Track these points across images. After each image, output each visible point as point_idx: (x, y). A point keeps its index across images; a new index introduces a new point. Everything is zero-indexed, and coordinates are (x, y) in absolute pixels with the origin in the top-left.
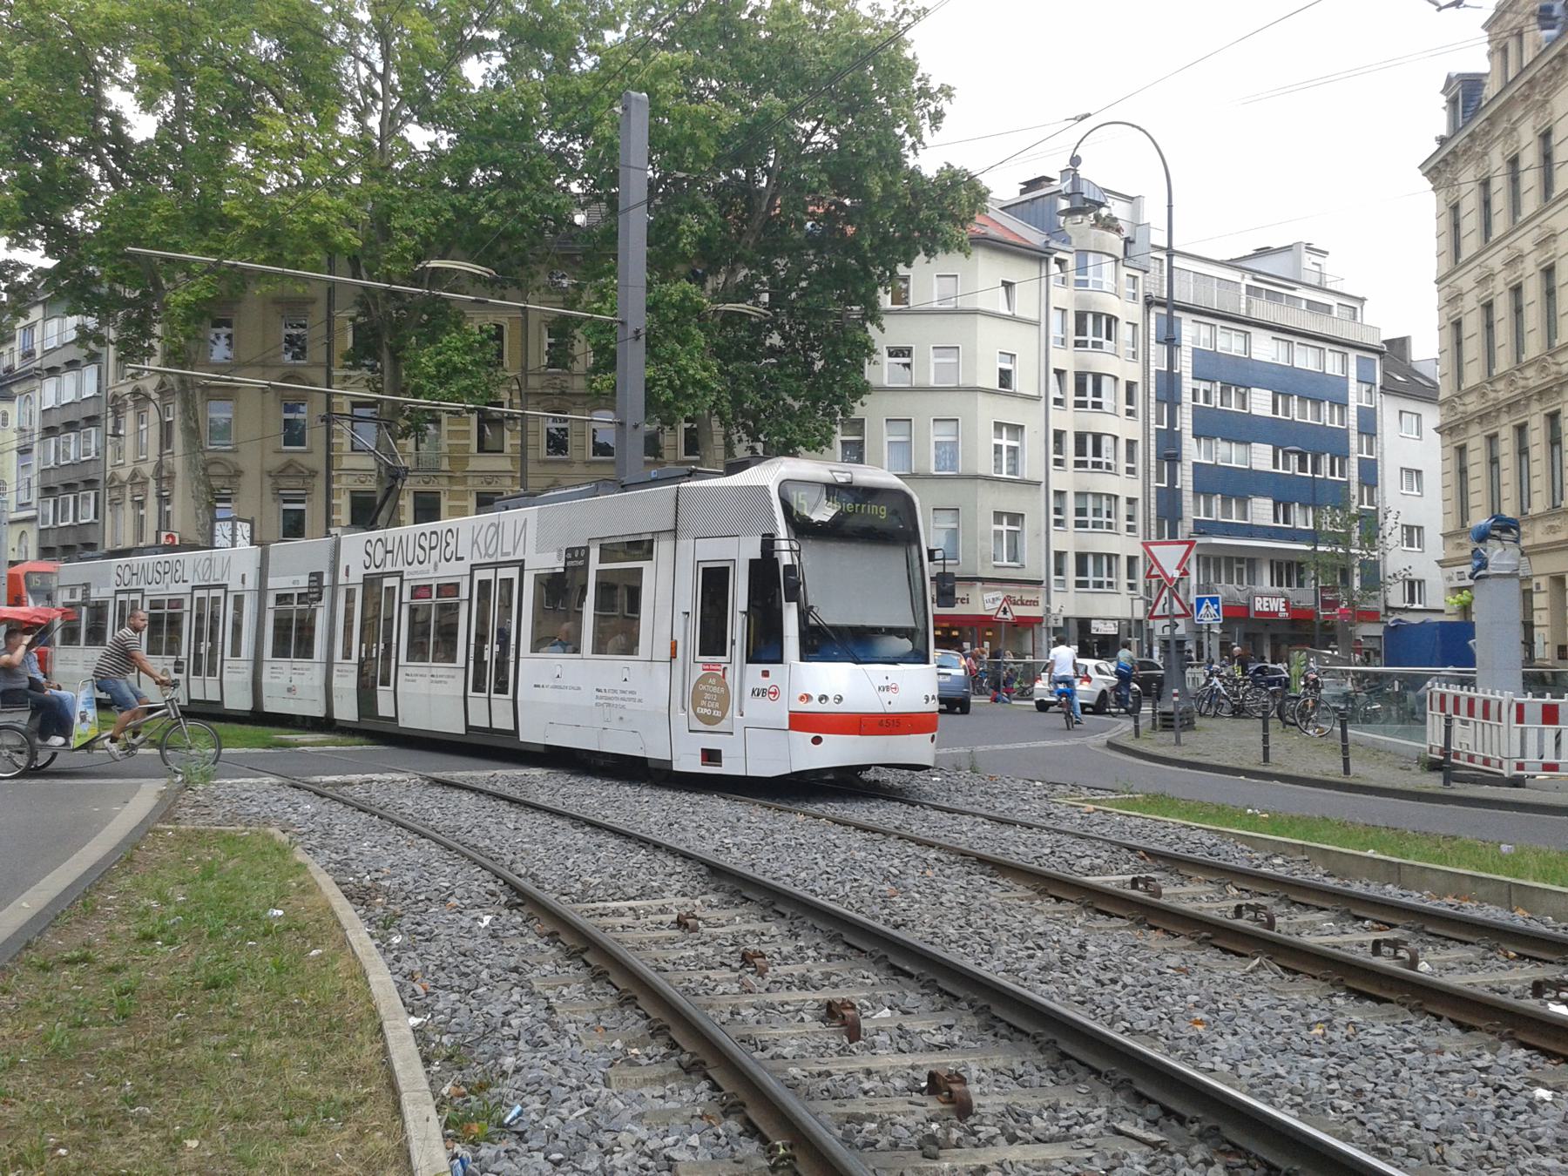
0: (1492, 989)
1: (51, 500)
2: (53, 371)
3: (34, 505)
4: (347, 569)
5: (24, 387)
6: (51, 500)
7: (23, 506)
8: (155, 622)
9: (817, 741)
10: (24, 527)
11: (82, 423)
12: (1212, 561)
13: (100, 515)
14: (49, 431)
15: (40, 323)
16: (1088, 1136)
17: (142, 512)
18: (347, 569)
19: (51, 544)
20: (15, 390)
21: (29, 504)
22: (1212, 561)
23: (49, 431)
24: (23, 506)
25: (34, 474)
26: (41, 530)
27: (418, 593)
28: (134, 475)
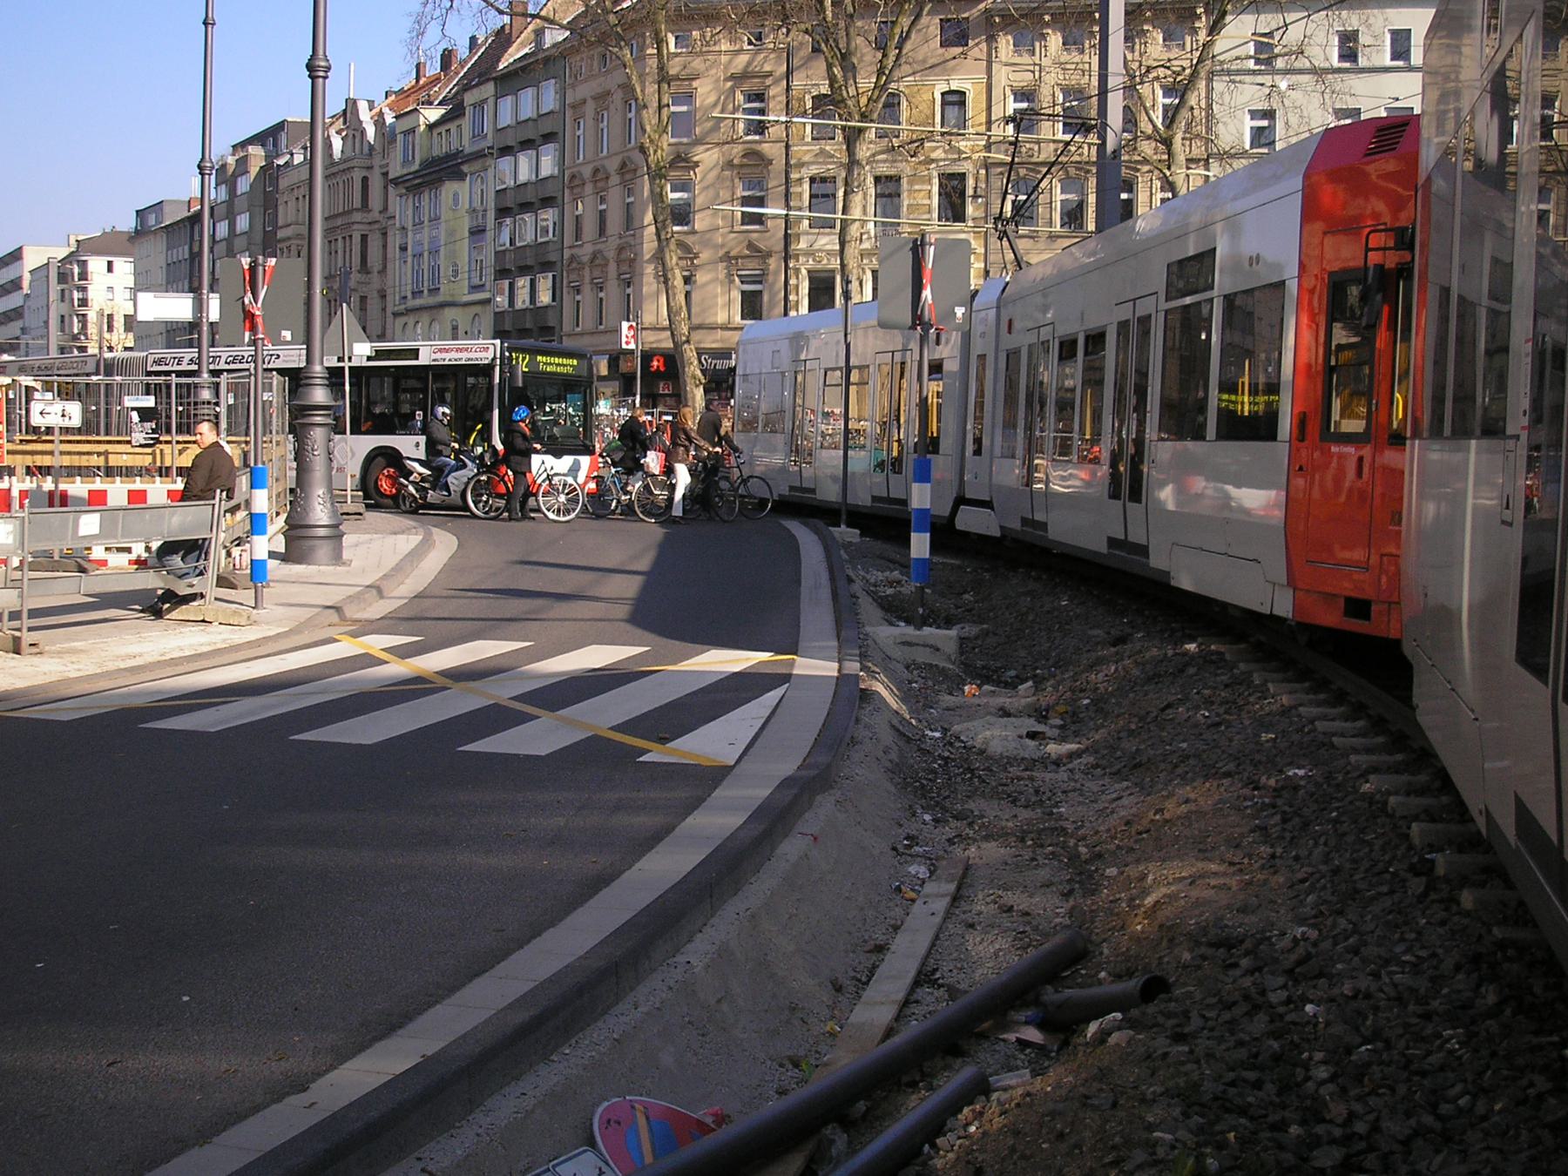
1: (507, 282)
2: (506, 151)
3: (488, 287)
4: (1010, 322)
5: (477, 165)
6: (507, 282)
7: (475, 288)
9: (1358, 608)
10: (477, 309)
12: (1265, 123)
13: (558, 299)
14: (503, 212)
15: (491, 101)
17: (578, 298)
18: (1010, 322)
19: (508, 327)
20: (465, 168)
21: (483, 286)
22: (1265, 123)
23: (503, 212)
24: (475, 288)
25: (489, 258)
26: (496, 314)
27: (1407, 240)
28: (594, 256)
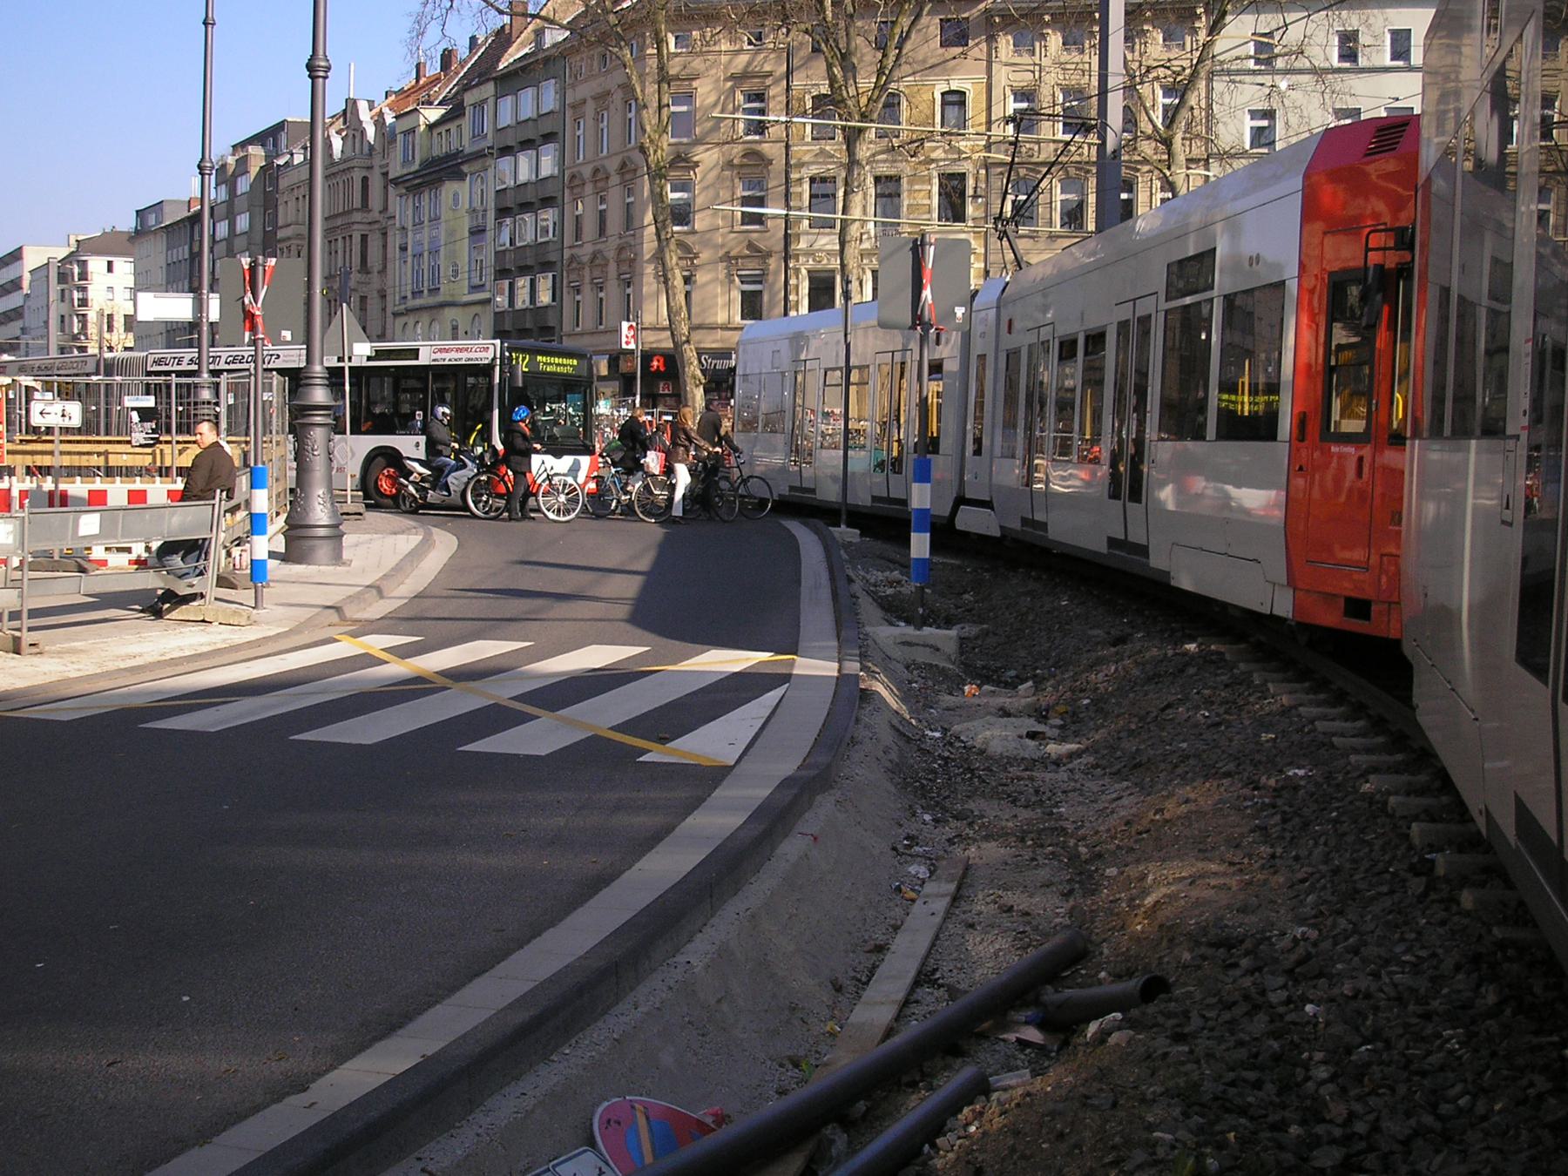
0: (1240, 82)
1: (507, 282)
2: (506, 151)
3: (488, 287)
5: (477, 165)
6: (507, 282)
7: (475, 288)
8: (650, 377)
10: (477, 309)
11: (516, 210)
12: (1265, 123)
13: (558, 299)
14: (503, 212)
15: (491, 101)
16: (1333, 1141)
17: (578, 298)
19: (508, 327)
20: (465, 168)
21: (483, 286)
22: (1265, 123)
23: (503, 212)
24: (475, 288)
25: (489, 258)
26: (496, 314)
28: (594, 256)
